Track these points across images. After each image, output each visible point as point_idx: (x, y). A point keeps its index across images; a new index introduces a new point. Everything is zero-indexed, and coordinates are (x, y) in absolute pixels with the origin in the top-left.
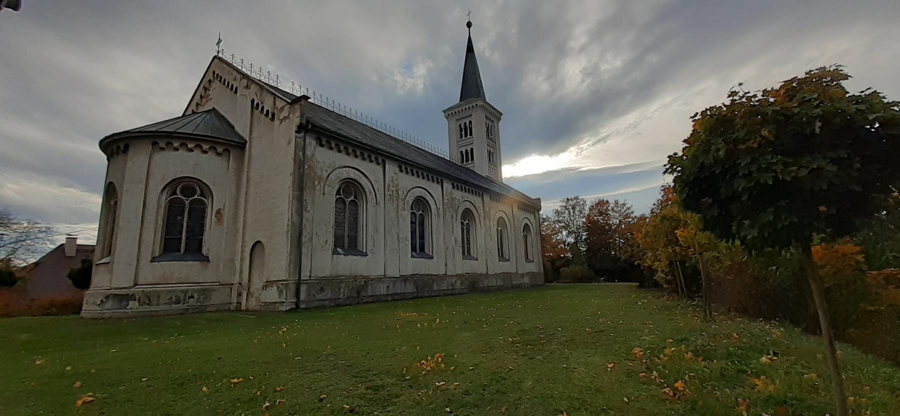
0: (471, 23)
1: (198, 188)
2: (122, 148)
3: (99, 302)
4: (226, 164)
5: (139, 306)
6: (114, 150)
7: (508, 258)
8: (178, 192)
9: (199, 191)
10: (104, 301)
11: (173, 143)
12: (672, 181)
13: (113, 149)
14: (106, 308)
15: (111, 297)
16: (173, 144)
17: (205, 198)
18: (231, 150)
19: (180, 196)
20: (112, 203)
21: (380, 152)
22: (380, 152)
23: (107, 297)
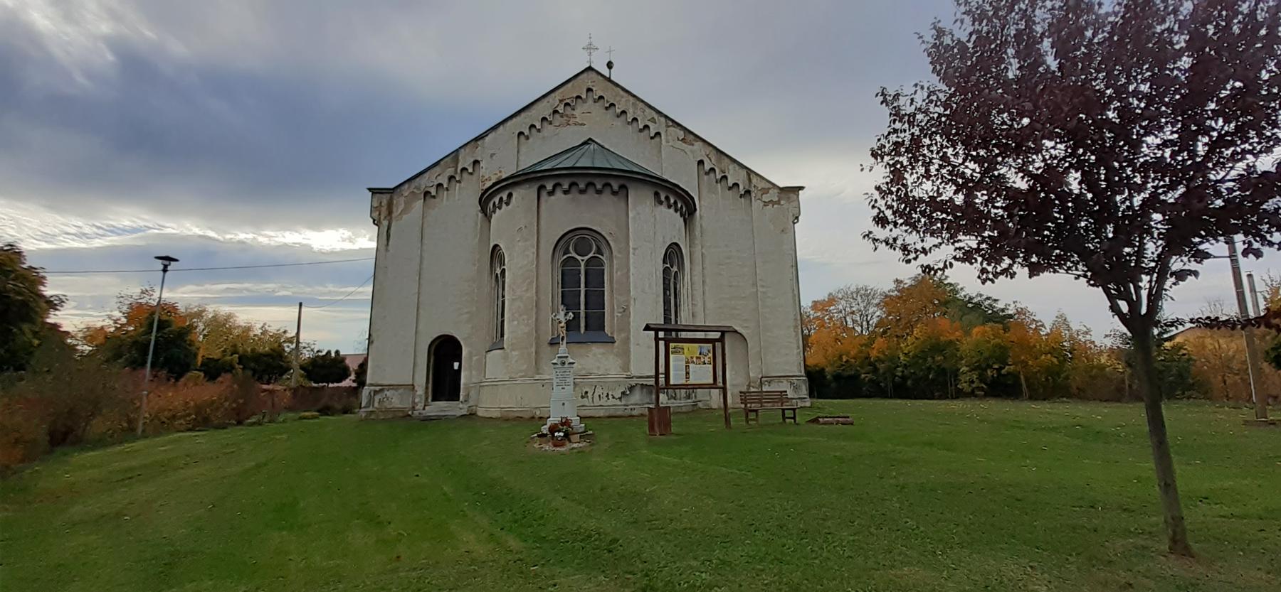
0: (612, 63)
1: (593, 243)
2: (505, 198)
3: (618, 395)
4: (623, 205)
5: (669, 399)
6: (497, 203)
7: (720, 333)
8: (571, 249)
9: (594, 248)
10: (628, 392)
11: (578, 183)
12: (1262, 170)
13: (494, 203)
14: (632, 402)
15: (638, 388)
16: (578, 185)
17: (602, 255)
18: (628, 185)
19: (574, 255)
20: (498, 271)
21: (678, 190)
22: (678, 190)
23: (631, 388)
